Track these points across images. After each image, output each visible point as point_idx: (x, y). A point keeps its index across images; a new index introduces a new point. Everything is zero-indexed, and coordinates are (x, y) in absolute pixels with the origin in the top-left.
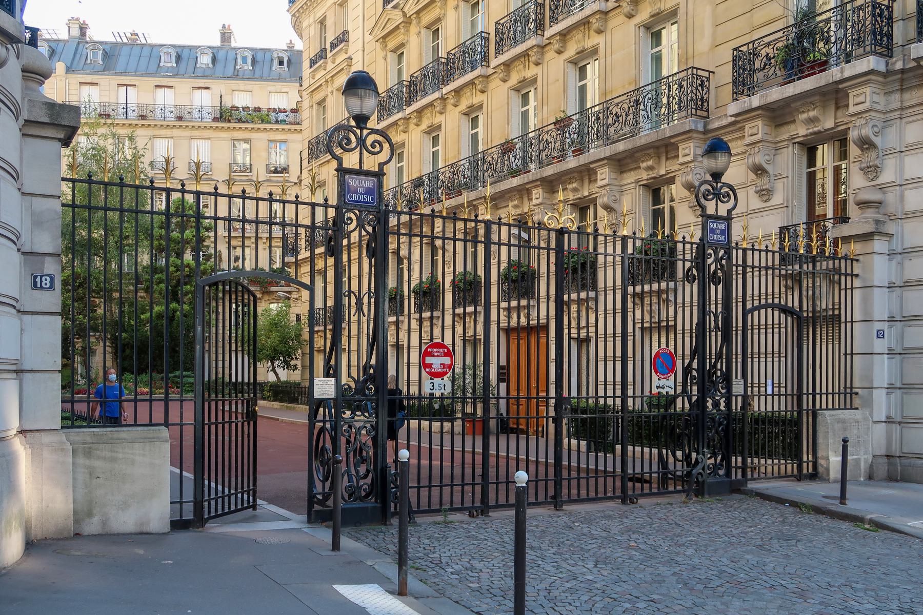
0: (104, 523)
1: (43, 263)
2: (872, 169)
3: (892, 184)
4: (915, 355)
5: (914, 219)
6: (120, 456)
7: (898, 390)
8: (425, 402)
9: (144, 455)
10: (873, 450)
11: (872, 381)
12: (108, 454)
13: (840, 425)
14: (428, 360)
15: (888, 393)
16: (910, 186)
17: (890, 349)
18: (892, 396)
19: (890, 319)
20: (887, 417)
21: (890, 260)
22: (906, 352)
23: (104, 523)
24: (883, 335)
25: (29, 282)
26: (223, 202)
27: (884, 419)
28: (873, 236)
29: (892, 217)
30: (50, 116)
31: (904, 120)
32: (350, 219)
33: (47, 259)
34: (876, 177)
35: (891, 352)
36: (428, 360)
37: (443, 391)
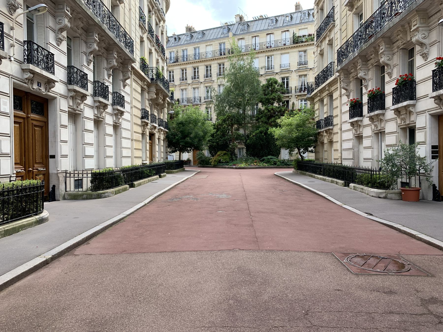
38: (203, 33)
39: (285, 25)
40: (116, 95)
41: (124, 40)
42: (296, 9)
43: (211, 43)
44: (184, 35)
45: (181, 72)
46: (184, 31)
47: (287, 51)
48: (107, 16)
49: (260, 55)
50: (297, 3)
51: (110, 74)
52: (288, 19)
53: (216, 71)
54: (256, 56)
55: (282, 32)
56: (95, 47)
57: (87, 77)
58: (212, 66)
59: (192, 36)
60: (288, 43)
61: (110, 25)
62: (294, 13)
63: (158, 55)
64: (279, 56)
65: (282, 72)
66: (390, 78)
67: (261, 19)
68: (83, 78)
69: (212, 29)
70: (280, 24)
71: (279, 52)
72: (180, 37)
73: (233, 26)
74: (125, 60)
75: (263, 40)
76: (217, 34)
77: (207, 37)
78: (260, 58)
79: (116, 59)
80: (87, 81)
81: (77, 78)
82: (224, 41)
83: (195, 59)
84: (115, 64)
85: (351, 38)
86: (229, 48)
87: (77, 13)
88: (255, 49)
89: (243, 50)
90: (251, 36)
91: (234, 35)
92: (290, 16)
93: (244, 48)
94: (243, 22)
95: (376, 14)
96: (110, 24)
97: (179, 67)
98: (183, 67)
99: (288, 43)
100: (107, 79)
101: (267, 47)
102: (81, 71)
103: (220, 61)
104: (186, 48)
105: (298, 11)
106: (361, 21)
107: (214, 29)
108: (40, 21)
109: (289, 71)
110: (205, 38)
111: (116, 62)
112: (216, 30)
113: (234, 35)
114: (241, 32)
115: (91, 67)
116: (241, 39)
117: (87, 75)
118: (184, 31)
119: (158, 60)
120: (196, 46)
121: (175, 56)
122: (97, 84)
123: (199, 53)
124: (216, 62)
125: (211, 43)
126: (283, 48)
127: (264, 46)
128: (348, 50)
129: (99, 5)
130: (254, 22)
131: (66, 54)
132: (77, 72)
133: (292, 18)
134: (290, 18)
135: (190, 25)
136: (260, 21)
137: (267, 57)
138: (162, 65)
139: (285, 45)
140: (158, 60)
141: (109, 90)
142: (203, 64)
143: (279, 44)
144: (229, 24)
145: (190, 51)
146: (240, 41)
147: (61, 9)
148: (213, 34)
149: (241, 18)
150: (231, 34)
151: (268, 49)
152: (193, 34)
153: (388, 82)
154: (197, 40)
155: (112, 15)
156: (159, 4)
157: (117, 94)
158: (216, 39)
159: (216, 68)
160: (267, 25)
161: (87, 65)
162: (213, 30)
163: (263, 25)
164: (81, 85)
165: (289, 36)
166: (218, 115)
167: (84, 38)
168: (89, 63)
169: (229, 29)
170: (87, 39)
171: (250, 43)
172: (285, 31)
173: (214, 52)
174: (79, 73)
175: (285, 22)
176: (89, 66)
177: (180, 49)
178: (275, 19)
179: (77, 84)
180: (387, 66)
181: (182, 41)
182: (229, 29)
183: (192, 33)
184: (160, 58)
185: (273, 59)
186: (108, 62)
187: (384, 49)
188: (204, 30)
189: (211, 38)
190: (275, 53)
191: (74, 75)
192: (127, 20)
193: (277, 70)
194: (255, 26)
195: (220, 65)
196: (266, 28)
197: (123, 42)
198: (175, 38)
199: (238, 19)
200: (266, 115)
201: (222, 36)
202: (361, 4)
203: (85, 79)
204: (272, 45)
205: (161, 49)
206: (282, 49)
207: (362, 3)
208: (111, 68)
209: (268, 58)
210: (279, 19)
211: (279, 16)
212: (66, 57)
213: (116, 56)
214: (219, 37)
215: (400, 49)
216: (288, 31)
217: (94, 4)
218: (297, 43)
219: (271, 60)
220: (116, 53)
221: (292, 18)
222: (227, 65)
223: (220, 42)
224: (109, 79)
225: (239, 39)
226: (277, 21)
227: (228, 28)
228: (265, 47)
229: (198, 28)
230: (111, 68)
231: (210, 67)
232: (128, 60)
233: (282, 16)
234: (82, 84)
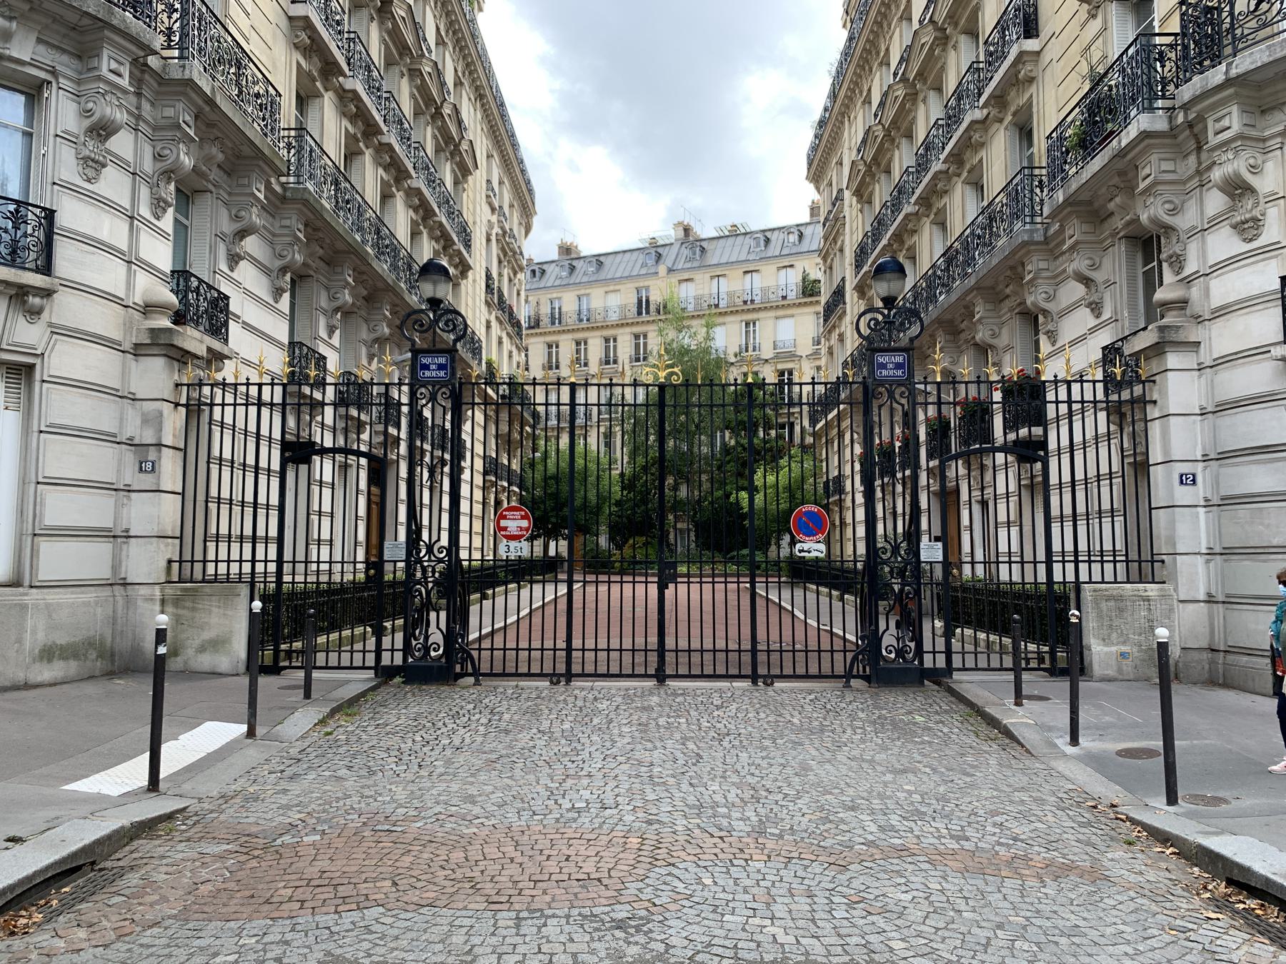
0: (186, 663)
1: (148, 452)
2: (1174, 259)
3: (1196, 276)
4: (1248, 506)
5: (1221, 318)
6: (200, 606)
7: (1218, 557)
8: (707, 569)
9: (219, 607)
10: (1180, 641)
11: (1174, 545)
12: (191, 605)
13: (1112, 603)
14: (503, 523)
15: (1208, 561)
16: (1215, 274)
17: (1207, 500)
18: (1212, 565)
19: (1205, 458)
20: (1209, 595)
21: (1200, 377)
22: (1230, 501)
23: (186, 663)
24: (1194, 480)
25: (137, 468)
26: (593, 391)
27: (1202, 597)
28: (1164, 347)
29: (1198, 319)
30: (152, 338)
31: (1205, 188)
32: (881, 393)
33: (151, 448)
34: (1181, 268)
35: (1208, 504)
36: (503, 523)
37: (519, 554)
38: (599, 261)
39: (784, 252)
40: (297, 351)
41: (333, 192)
42: (812, 215)
43: (617, 287)
44: (554, 264)
45: (547, 350)
46: (554, 255)
47: (789, 312)
48: (329, 179)
49: (729, 319)
50: (813, 202)
51: (334, 326)
52: (793, 238)
53: (628, 350)
54: (721, 320)
55: (779, 269)
56: (347, 297)
57: (228, 305)
58: (619, 339)
59: (572, 268)
60: (792, 295)
61: (337, 202)
62: (807, 224)
63: (512, 344)
64: (771, 323)
65: (777, 356)
66: (1097, 317)
67: (735, 233)
68: (217, 306)
69: (619, 252)
70: (774, 249)
71: (772, 314)
72: (545, 267)
73: (668, 248)
74: (335, 253)
75: (734, 285)
76: (631, 264)
77: (608, 272)
78: (729, 326)
79: (389, 320)
80: (227, 315)
81: (197, 306)
82: (646, 284)
83: (581, 320)
84: (387, 330)
85: (1002, 194)
86: (659, 299)
87: (314, 230)
88: (717, 306)
89: (691, 308)
90: (707, 276)
91: (670, 270)
92: (797, 233)
93: (692, 300)
94: (691, 238)
95: (1125, 60)
96: (336, 198)
97: (542, 339)
98: (549, 339)
99: (792, 295)
100: (226, 269)
101: (745, 302)
102: (210, 287)
103: (637, 329)
104: (559, 295)
105: (815, 219)
106: (1028, 150)
107: (625, 252)
108: (746, 631)
109: (792, 356)
110: (602, 275)
111: (388, 326)
112: (628, 255)
113: (670, 270)
114: (689, 265)
115: (336, 340)
116: (687, 280)
117: (227, 298)
118: (554, 255)
119: (511, 352)
120: (583, 292)
121: (532, 313)
122: (181, 280)
123: (589, 310)
124: (628, 330)
125: (617, 287)
126: (782, 306)
127: (737, 300)
128: (995, 229)
129: (311, 151)
130: (715, 242)
131: (171, 238)
132: (198, 288)
133: (801, 236)
134: (797, 237)
135: (568, 240)
136: (731, 240)
137: (744, 324)
138: (499, 333)
139: (784, 298)
140: (511, 352)
141: (328, 366)
142: (598, 333)
143: (771, 296)
144: (661, 242)
145: (569, 303)
146: (684, 285)
147: (244, 185)
148: (623, 265)
149: (687, 230)
150: (662, 269)
151: (746, 307)
152: (574, 263)
153: (1050, 356)
154: (585, 279)
155: (346, 179)
156: (495, 195)
157: (300, 349)
158: (629, 277)
159: (628, 344)
160: (746, 249)
161: (272, 302)
162: (621, 255)
163: (737, 249)
164: (207, 328)
165: (792, 279)
166: (633, 454)
167: (363, 313)
168: (331, 332)
169: (659, 256)
170: (369, 314)
171: (706, 292)
172: (785, 267)
173: (623, 308)
174: (202, 291)
175: (786, 244)
176: (232, 271)
177: (544, 298)
178: (762, 238)
179: (197, 324)
180: (1043, 314)
181: (550, 279)
182: (659, 256)
183: (572, 259)
184: (504, 335)
185: (757, 328)
186: (371, 326)
187: (1153, 176)
188: (599, 255)
189: (618, 275)
190: (761, 315)
191: (190, 296)
192: (470, 303)
193: (767, 353)
194: (718, 252)
195: (637, 337)
196: (743, 257)
197: (372, 246)
198: (534, 272)
199: (682, 233)
200: (739, 458)
201: (644, 271)
202: (1028, 100)
203: (221, 312)
204: (755, 298)
205: (507, 314)
206: (777, 306)
207: (1031, 96)
208: (337, 310)
209: (747, 325)
210: (774, 237)
211: (774, 230)
212: (170, 244)
213: (350, 280)
214: (635, 273)
215: (1120, 239)
216: (791, 266)
217: (259, 101)
218: (811, 295)
219: (754, 331)
220: (351, 272)
221: (801, 236)
222: (654, 343)
223: (637, 285)
224: (276, 302)
225: (680, 282)
226: (767, 241)
227: (655, 251)
228: (739, 302)
229: (588, 246)
230: (337, 310)
231: (615, 340)
232: (344, 252)
233: (779, 229)
234: (211, 325)
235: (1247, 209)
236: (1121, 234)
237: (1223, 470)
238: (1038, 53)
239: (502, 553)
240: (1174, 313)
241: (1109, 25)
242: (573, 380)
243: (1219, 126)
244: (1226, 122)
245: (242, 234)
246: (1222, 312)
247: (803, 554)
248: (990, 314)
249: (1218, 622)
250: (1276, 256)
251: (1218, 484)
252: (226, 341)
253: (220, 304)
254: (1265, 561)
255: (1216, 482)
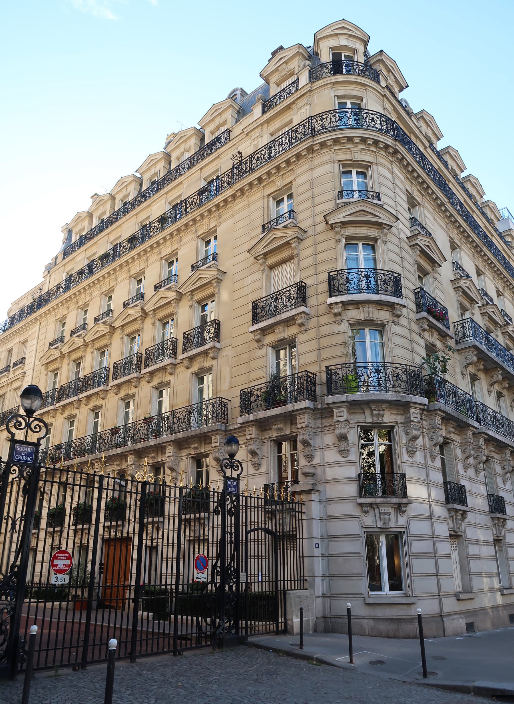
3: (319, 465)
14: (56, 562)
15: (322, 580)
20: (323, 594)
27: (321, 595)
31: (323, 433)
34: (312, 461)
36: (56, 562)
37: (63, 583)
235: (343, 445)
236: (272, 439)
237: (330, 543)
238: (219, 349)
239: (53, 581)
240: (310, 478)
241: (268, 355)
242: (102, 473)
243: (338, 414)
244: (342, 414)
245: (468, 458)
246: (332, 481)
247: (199, 580)
248: (175, 454)
249: (327, 605)
250: (354, 465)
251: (328, 548)
252: (467, 506)
253: (462, 489)
254: (349, 580)
255: (328, 547)
